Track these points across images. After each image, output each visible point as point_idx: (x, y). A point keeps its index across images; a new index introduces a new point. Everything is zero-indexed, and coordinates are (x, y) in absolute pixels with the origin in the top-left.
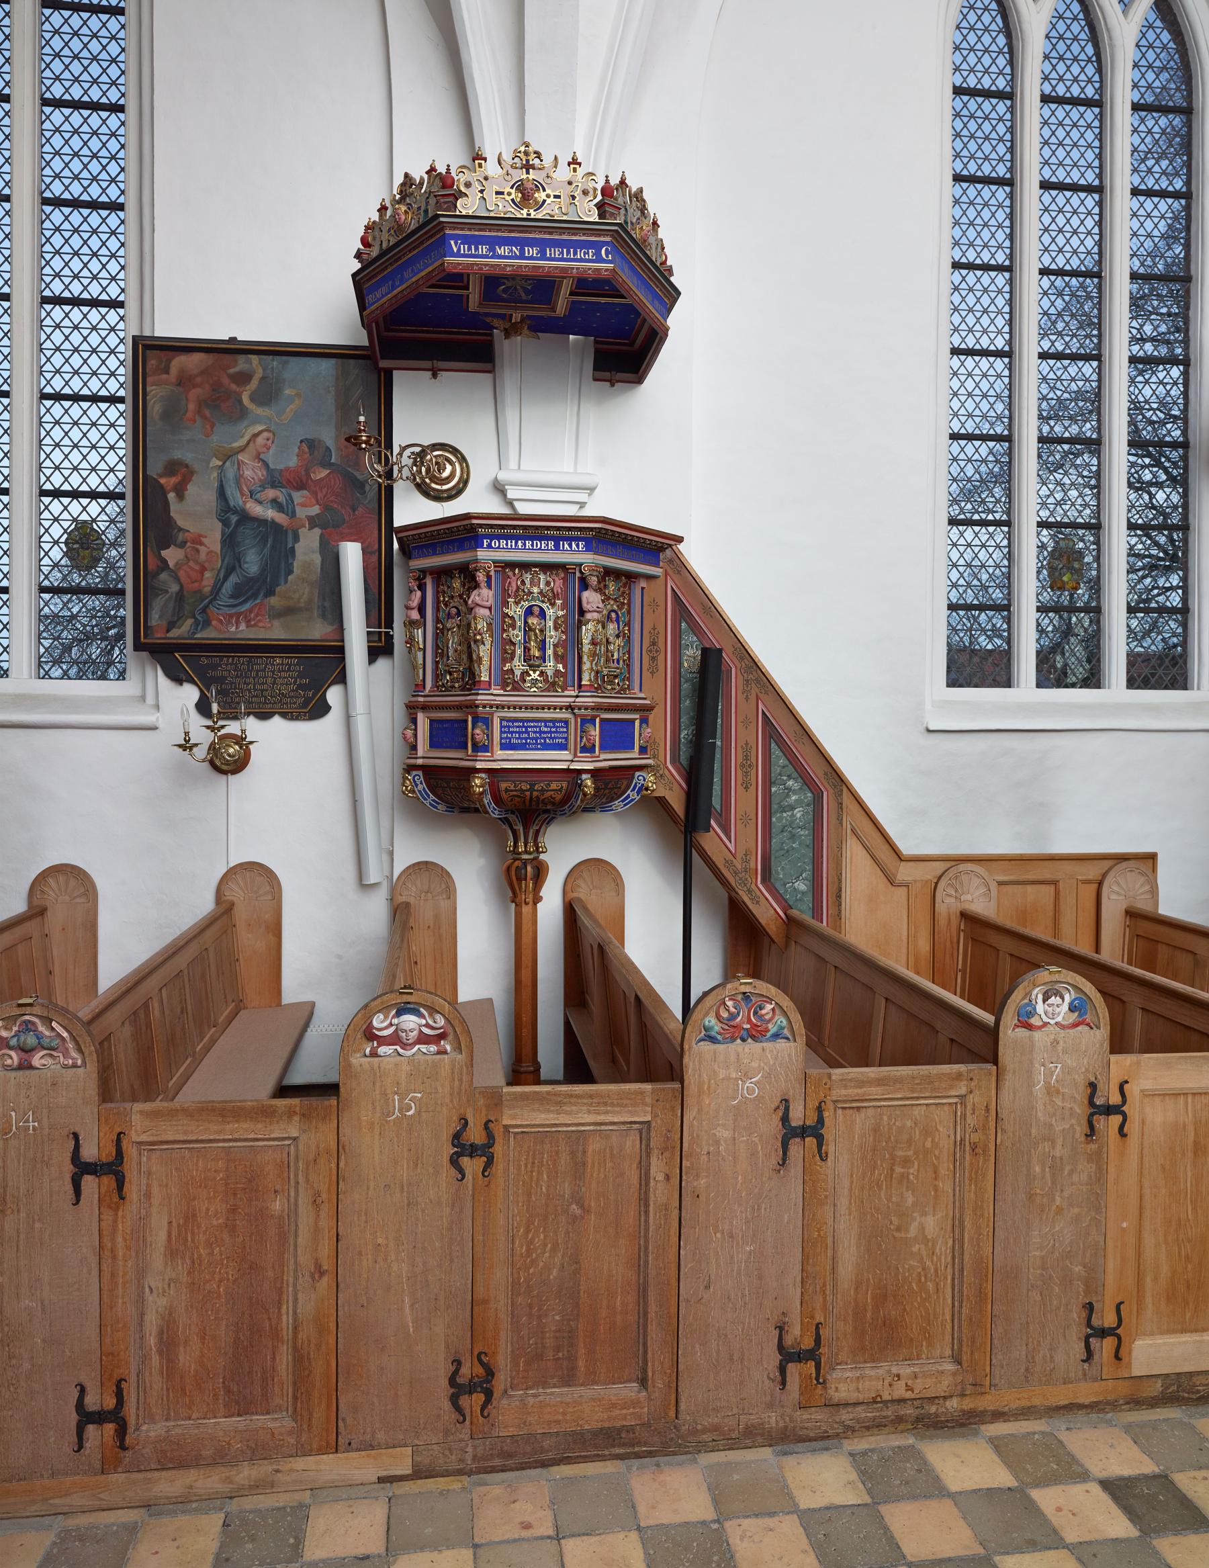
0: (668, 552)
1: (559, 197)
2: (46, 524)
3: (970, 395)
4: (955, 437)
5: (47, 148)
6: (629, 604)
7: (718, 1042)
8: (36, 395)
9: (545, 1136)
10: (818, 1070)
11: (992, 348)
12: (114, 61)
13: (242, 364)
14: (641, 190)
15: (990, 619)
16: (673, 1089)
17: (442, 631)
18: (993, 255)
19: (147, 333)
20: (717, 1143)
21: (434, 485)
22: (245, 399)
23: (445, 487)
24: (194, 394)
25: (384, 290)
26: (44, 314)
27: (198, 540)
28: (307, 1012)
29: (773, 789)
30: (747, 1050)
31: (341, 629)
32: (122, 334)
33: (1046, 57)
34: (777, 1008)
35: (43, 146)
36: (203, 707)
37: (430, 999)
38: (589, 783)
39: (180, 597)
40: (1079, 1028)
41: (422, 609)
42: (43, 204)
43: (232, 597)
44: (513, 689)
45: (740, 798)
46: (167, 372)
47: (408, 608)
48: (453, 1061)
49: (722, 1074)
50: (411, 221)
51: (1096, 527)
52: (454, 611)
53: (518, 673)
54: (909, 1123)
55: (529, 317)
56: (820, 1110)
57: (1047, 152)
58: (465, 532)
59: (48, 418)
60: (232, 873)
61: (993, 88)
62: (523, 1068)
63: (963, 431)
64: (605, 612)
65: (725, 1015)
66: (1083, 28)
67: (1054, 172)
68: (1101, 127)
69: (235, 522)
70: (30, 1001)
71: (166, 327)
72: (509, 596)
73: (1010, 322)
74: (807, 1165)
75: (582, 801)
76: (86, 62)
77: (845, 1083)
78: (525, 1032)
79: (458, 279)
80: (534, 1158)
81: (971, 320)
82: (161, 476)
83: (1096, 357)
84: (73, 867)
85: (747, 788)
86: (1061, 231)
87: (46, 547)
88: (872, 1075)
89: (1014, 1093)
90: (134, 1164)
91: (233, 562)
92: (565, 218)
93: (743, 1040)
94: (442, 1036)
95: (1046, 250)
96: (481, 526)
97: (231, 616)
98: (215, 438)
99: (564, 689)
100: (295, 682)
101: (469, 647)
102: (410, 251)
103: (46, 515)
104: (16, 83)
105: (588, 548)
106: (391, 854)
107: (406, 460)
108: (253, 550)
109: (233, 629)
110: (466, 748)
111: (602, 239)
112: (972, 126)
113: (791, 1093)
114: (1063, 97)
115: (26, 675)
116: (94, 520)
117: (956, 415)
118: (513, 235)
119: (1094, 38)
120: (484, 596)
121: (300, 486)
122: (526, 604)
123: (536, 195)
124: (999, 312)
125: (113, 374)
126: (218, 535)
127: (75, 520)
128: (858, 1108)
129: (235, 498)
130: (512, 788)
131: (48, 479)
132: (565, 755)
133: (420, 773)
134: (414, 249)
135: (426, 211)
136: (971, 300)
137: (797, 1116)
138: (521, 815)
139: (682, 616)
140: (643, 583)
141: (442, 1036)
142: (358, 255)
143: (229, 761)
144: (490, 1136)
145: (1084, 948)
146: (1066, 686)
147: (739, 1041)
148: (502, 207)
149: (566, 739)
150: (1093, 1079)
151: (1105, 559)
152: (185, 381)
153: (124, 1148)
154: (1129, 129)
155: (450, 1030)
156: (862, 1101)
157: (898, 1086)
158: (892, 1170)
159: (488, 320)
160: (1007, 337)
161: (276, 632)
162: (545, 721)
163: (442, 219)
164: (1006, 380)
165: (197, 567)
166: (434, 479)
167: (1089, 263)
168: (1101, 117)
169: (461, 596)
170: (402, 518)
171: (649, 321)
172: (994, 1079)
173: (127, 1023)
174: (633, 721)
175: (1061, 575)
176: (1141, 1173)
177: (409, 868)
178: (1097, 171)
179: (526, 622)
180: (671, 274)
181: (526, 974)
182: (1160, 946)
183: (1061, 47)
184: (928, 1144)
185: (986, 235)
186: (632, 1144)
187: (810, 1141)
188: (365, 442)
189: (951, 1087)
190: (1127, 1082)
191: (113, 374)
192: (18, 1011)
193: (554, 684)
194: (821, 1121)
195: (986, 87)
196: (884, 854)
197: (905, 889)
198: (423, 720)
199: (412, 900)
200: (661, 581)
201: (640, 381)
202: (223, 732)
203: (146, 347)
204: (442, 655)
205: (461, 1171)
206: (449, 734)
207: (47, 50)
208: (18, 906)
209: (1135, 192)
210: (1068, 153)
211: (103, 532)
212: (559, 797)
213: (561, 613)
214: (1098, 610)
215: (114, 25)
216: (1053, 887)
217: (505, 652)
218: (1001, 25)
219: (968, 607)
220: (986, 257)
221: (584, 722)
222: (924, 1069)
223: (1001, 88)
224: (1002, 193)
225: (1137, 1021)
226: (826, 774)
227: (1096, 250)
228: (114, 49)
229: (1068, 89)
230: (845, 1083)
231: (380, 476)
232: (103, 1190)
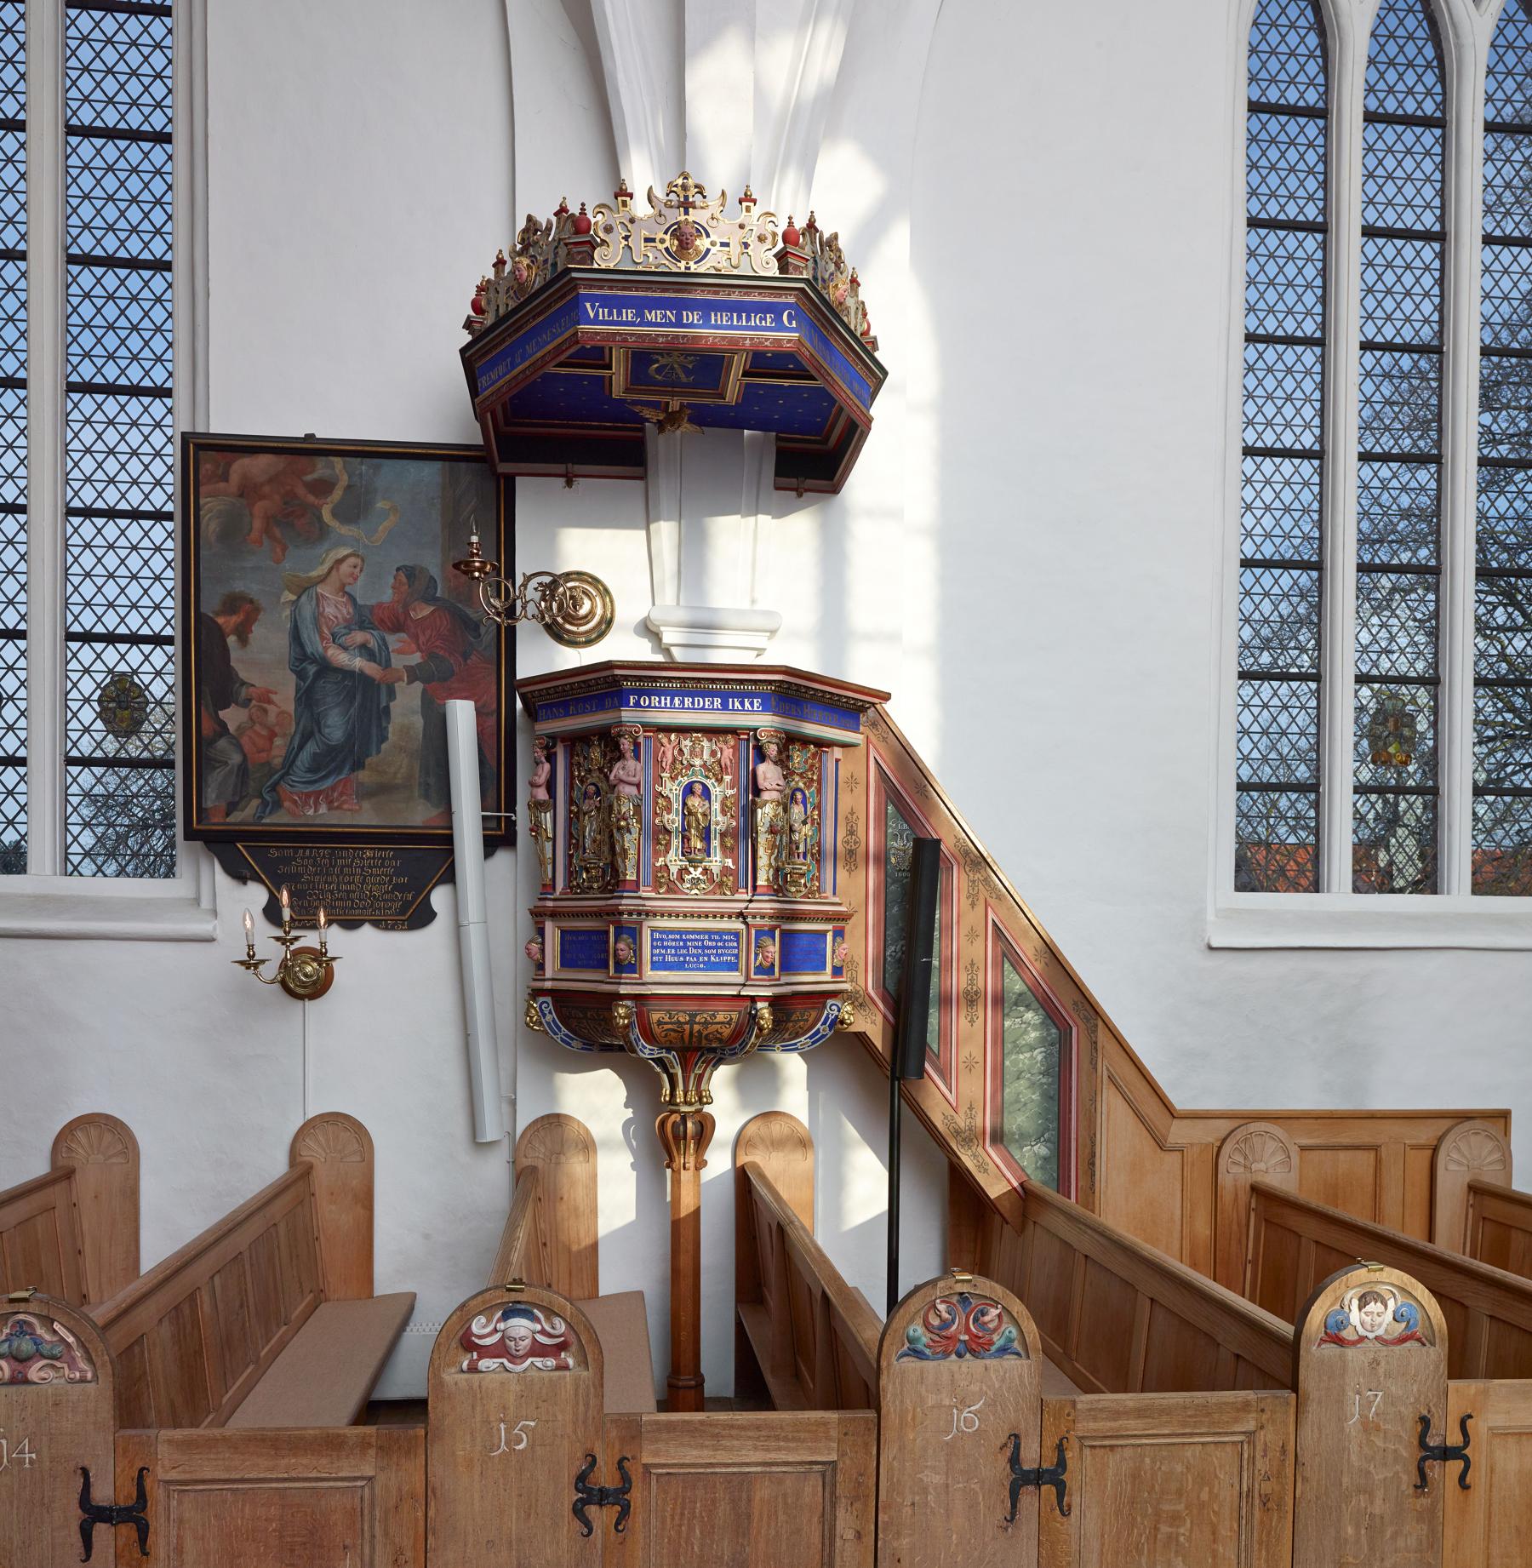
0: (871, 712)
1: (727, 245)
2: (74, 676)
3: (1267, 508)
4: (1247, 563)
5: (74, 190)
6: (819, 781)
7: (927, 1358)
8: (61, 510)
9: (695, 1479)
10: (1061, 1392)
11: (1298, 446)
12: (158, 76)
13: (321, 468)
14: (835, 237)
15: (1293, 804)
16: (867, 1420)
17: (577, 814)
18: (1299, 324)
19: (200, 429)
20: (925, 1491)
21: (568, 626)
22: (326, 514)
23: (582, 629)
24: (260, 507)
25: (501, 369)
26: (70, 405)
27: (266, 698)
28: (408, 1306)
29: (1007, 1024)
30: (964, 1369)
31: (448, 812)
32: (169, 431)
33: (1372, 61)
34: (1009, 1318)
35: (68, 188)
36: (272, 912)
37: (545, 1296)
38: (766, 1013)
39: (243, 771)
40: (1408, 1344)
41: (551, 786)
42: (68, 262)
43: (310, 770)
44: (667, 892)
45: (962, 1036)
46: (227, 480)
47: (533, 785)
48: (577, 1380)
49: (931, 1400)
50: (534, 278)
51: (1432, 681)
52: (592, 789)
53: (674, 869)
54: (1179, 1468)
55: (690, 406)
56: (1060, 1449)
57: (1371, 188)
58: (607, 685)
59: (75, 540)
60: (309, 1127)
61: (1301, 103)
62: (681, 1388)
63: (1258, 556)
64: (788, 791)
65: (936, 1322)
66: (1420, 23)
67: (1380, 215)
68: (1443, 154)
69: (313, 674)
70: (25, 1294)
71: (223, 422)
72: (664, 770)
73: (1322, 413)
74: (1044, 1521)
75: (757, 1037)
76: (122, 78)
77: (1094, 1413)
78: (684, 1335)
79: (596, 356)
80: (683, 1508)
81: (1269, 410)
82: (218, 614)
83: (1434, 459)
84: (108, 1117)
86: (1389, 292)
87: (74, 706)
88: (1131, 1404)
89: (1320, 1430)
90: (161, 1508)
91: (310, 728)
92: (735, 272)
93: (960, 1356)
94: (563, 1346)
95: (1370, 317)
96: (626, 678)
97: (308, 795)
98: (287, 565)
99: (734, 891)
101: (611, 836)
102: (534, 318)
103: (74, 665)
104: (33, 107)
105: (765, 708)
106: (513, 1103)
107: (532, 593)
108: (336, 711)
109: (311, 812)
110: (607, 966)
111: (783, 300)
112: (1273, 154)
113: (1022, 1426)
114: (1393, 114)
115: (48, 871)
116: (135, 672)
117: (1249, 534)
118: (667, 295)
119: (1436, 36)
121: (397, 628)
122: (685, 781)
123: (698, 242)
124: (1307, 399)
125: (158, 483)
126: (291, 692)
127: (110, 671)
128: (1112, 1447)
130: (667, 1019)
131: (76, 618)
132: (736, 977)
133: (549, 999)
134: (539, 314)
135: (554, 265)
136: (1270, 383)
137: (1031, 1457)
138: (673, 1056)
141: (563, 1346)
142: (468, 325)
143: (306, 982)
144: (626, 1479)
145: (1413, 1236)
146: (1393, 891)
147: (954, 1357)
148: (652, 258)
149: (737, 956)
150: (1425, 1412)
151: (1444, 725)
152: (249, 491)
153: (148, 1488)
154: (1480, 156)
155: (572, 1339)
156: (1117, 1437)
157: (1164, 1418)
158: (1156, 1529)
159: (637, 409)
160: (1317, 431)
161: (366, 816)
162: (709, 932)
163: (574, 275)
164: (1316, 489)
165: (264, 732)
166: (570, 619)
167: (1427, 333)
168: (1443, 141)
169: (600, 770)
170: (526, 667)
171: (846, 409)
172: (1292, 1410)
173: (166, 1323)
174: (824, 934)
175: (1386, 746)
176: (1488, 1537)
178: (1438, 212)
179: (684, 804)
180: (876, 348)
181: (685, 1261)
182: (1514, 1233)
183: (1392, 49)
184: (1205, 1496)
185: (1290, 297)
186: (811, 1490)
187: (1048, 1490)
188: (479, 570)
189: (1236, 1421)
190: (1470, 1417)
191: (158, 483)
192: (9, 1309)
193: (721, 884)
194: (1062, 1463)
195: (1292, 102)
196: (1151, 1108)
197: (1178, 1154)
198: (552, 931)
199: (540, 1164)
201: (835, 489)
202: (297, 945)
203: (198, 447)
204: (577, 847)
205: (587, 1524)
206: (586, 948)
207: (73, 62)
208: (38, 1166)
209: (1488, 240)
210: (1400, 189)
211: (147, 687)
213: (730, 792)
214: (1435, 791)
215: (158, 29)
216: (1373, 1154)
218: (1312, 20)
219: (1265, 788)
220: (1290, 326)
221: (759, 934)
222: (1199, 1397)
223: (1311, 103)
224: (1311, 242)
225: (1484, 1334)
226: (1075, 1003)
227: (1436, 317)
228: (158, 60)
229: (1400, 104)
230: (1094, 1413)
231: (499, 614)
232: (121, 1543)
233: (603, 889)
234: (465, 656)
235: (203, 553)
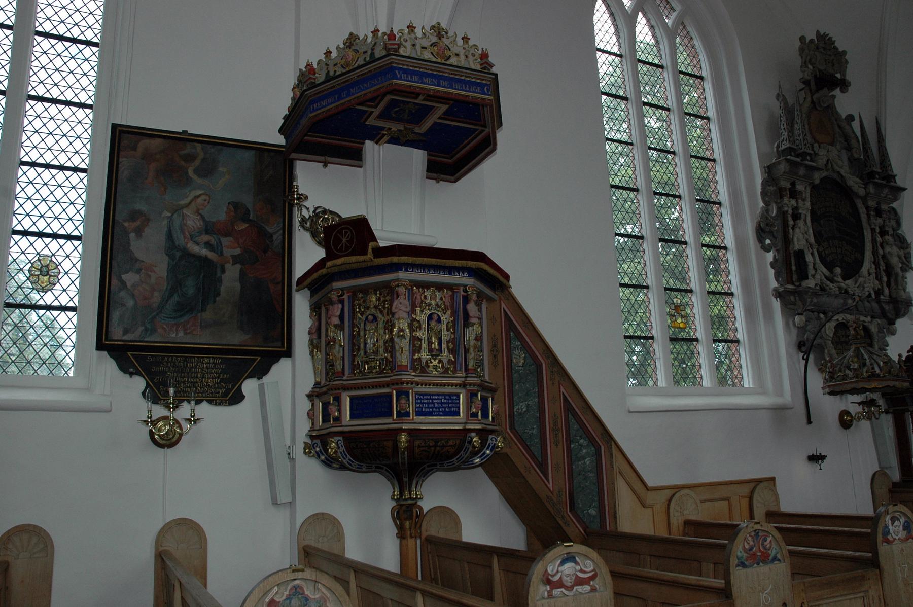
13: (188, 149)
43: (176, 311)
53: (424, 361)
65: (747, 546)
82: (125, 221)
93: (758, 564)
94: (593, 578)
99: (455, 372)
109: (174, 335)
110: (391, 415)
120: (401, 305)
121: (227, 235)
129: (180, 240)
133: (341, 438)
141: (593, 578)
152: (148, 157)
162: (444, 395)
179: (428, 325)
217: (414, 345)
233: (381, 372)
234: (265, 252)
235: (119, 187)
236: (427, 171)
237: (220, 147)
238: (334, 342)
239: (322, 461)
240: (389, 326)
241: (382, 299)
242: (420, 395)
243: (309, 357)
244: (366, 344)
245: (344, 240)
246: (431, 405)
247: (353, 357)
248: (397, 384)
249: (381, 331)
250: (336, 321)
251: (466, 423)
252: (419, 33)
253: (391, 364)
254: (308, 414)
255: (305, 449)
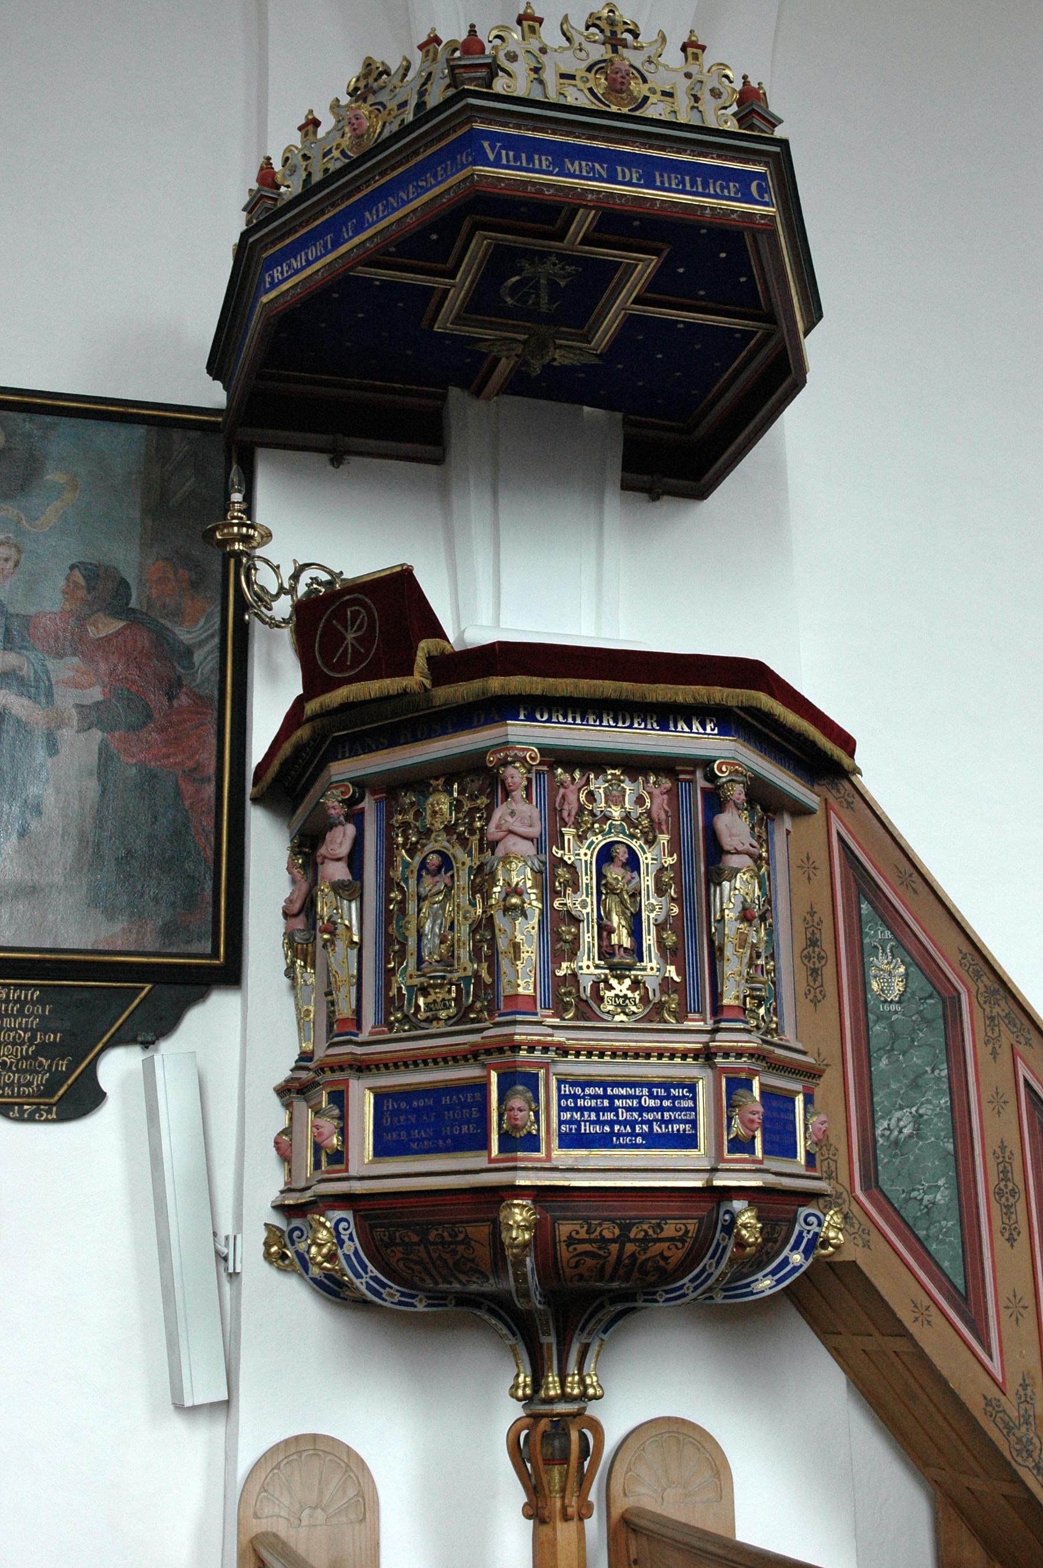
38: (747, 1218)
52: (434, 860)
53: (587, 983)
85: (1011, 1240)
99: (681, 1015)
100: (32, 1039)
120: (518, 815)
122: (600, 841)
130: (583, 1235)
133: (348, 1215)
139: (860, 891)
140: (787, 822)
149: (694, 1123)
177: (277, 1446)
179: (600, 876)
200: (818, 818)
201: (702, 494)
212: (676, 1255)
217: (558, 937)
233: (462, 1017)
236: (623, 470)
237: (48, 419)
238: (333, 933)
239: (313, 1280)
240: (482, 880)
241: (467, 806)
242: (573, 1084)
243: (286, 981)
244: (420, 936)
245: (350, 636)
246: (610, 1116)
247: (387, 975)
248: (501, 1050)
249: (464, 899)
250: (339, 872)
251: (714, 1170)
252: (550, 35)
253: (485, 998)
254: (277, 1143)
255: (267, 1245)
